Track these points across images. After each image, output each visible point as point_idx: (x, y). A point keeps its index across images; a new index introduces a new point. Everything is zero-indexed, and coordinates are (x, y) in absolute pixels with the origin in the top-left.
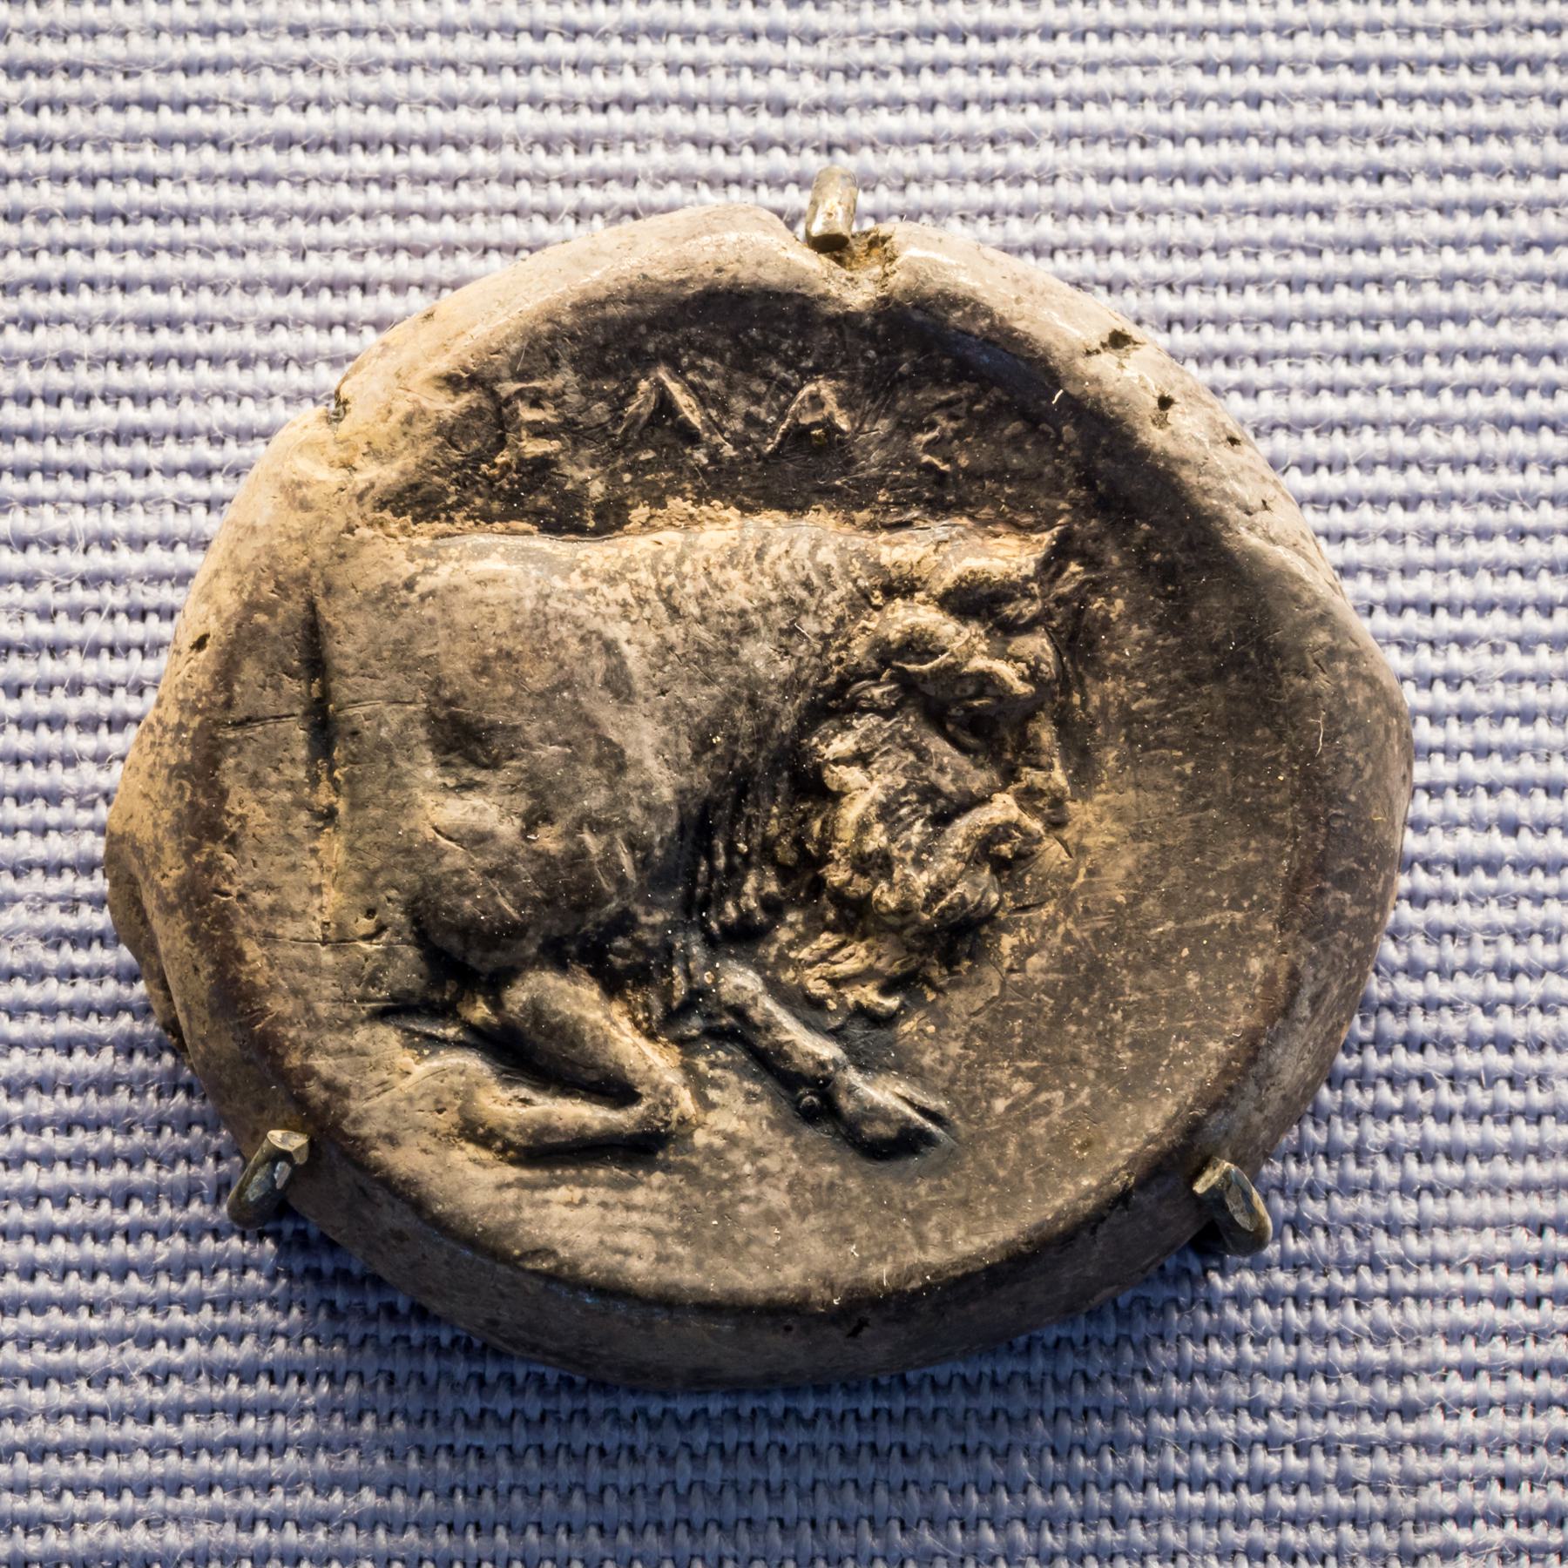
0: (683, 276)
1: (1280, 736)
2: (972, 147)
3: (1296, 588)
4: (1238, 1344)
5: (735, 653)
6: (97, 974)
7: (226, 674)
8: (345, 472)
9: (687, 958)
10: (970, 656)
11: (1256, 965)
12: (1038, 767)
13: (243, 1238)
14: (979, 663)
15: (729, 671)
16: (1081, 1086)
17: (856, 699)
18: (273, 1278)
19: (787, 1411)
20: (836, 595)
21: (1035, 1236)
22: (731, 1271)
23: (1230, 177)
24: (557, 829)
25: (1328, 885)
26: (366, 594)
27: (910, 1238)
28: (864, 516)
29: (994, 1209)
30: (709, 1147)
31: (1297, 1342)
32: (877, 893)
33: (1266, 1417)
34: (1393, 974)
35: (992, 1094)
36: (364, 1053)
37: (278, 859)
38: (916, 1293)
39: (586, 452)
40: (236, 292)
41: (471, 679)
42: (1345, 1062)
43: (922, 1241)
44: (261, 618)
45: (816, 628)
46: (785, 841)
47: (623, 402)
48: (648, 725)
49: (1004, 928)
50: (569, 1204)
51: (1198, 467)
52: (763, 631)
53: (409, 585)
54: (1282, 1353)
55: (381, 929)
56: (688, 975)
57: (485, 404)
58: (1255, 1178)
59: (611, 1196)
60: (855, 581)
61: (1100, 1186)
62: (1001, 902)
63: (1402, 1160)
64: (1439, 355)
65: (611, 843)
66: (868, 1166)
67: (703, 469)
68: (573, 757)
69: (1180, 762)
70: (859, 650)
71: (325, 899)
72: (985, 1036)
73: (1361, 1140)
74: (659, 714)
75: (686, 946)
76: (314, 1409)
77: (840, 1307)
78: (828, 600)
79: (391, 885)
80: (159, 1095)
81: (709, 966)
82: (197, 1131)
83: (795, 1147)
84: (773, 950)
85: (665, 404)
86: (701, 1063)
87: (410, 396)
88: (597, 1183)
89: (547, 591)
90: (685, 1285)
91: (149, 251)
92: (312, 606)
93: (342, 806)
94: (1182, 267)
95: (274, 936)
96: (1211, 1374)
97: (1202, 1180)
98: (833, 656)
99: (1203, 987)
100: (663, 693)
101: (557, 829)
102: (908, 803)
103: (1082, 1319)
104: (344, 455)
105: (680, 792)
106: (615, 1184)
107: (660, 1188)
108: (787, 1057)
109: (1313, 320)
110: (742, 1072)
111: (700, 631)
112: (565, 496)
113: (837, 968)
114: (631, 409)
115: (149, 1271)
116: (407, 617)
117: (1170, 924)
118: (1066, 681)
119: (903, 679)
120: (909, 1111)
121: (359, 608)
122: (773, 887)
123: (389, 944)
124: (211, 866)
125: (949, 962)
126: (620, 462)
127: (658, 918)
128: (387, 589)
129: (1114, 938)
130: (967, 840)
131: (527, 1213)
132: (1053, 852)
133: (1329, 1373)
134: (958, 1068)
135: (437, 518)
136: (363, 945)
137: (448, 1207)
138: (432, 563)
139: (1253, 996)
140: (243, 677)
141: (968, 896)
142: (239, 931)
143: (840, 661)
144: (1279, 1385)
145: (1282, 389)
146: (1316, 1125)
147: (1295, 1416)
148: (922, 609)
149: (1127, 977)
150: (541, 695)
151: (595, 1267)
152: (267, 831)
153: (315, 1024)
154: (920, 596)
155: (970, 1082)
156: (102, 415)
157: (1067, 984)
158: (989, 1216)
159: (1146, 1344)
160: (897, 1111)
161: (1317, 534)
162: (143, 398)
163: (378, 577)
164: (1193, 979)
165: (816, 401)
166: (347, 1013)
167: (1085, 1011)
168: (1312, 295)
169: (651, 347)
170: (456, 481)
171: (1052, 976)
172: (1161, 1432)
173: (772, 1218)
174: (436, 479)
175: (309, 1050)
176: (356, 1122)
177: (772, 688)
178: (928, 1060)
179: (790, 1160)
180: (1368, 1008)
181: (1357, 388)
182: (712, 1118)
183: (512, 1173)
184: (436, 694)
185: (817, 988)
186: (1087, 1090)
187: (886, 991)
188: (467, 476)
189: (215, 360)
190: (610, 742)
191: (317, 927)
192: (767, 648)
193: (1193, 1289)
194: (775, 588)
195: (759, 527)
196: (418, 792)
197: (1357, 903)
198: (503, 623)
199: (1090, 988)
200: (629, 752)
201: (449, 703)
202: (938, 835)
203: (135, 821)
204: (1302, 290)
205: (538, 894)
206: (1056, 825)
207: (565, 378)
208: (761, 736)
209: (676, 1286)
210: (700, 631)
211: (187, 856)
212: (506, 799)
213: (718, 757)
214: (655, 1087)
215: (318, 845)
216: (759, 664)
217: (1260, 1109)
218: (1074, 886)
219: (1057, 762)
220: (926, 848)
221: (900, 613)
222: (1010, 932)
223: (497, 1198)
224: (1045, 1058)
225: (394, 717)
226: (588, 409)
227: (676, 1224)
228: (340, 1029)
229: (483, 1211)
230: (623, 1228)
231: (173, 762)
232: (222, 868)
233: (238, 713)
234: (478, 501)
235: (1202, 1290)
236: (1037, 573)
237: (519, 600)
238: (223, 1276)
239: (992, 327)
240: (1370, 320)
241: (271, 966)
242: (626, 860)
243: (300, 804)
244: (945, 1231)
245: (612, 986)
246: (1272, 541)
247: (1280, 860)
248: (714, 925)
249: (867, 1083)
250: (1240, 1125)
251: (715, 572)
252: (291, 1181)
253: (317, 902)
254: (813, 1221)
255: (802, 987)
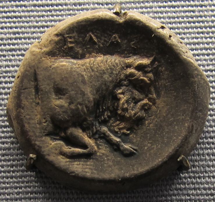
0: (93, 18)
1: (190, 88)
2: (139, 3)
3: (192, 65)
4: (185, 185)
5: (102, 77)
6: (7, 132)
7: (22, 81)
8: (40, 50)
9: (96, 125)
10: (140, 77)
11: (186, 125)
12: (151, 94)
13: (31, 172)
14: (142, 78)
15: (102, 79)
16: (159, 145)
17: (122, 84)
18: (35, 178)
19: (115, 197)
20: (119, 67)
21: (152, 168)
22: (103, 175)
23: (179, 7)
24: (74, 105)
25: (198, 112)
26: (43, 68)
27: (132, 169)
28: (123, 55)
29: (145, 164)
30: (99, 155)
31: (194, 184)
32: (126, 115)
33: (190, 196)
34: (208, 127)
35: (144, 146)
36: (44, 141)
37: (30, 111)
38: (133, 178)
39: (79, 46)
41: (60, 81)
42: (201, 141)
43: (134, 170)
44: (27, 73)
45: (115, 73)
46: (111, 107)
47: (85, 38)
48: (89, 88)
49: (146, 120)
50: (77, 165)
51: (176, 46)
52: (107, 73)
53: (50, 67)
54: (192, 186)
55: (46, 121)
56: (96, 128)
57: (62, 38)
58: (187, 158)
59: (84, 163)
60: (122, 66)
61: (162, 160)
62: (146, 116)
63: (210, 156)
64: (212, 33)
65: (83, 107)
66: (125, 158)
67: (97, 49)
68: (77, 93)
69: (174, 93)
70: (122, 76)
71: (38, 117)
72: (143, 137)
73: (203, 152)
74: (90, 86)
75: (96, 124)
76: (42, 198)
77: (120, 180)
78: (117, 68)
79: (48, 114)
80: (17, 150)
81: (99, 127)
82: (23, 156)
83: (113, 155)
84: (110, 124)
85: (91, 38)
86: (98, 142)
87: (51, 37)
88: (82, 161)
89: (72, 67)
90: (95, 177)
91: (14, 22)
92: (35, 70)
93: (40, 102)
94: (172, 20)
95: (30, 123)
96: (181, 189)
97: (179, 159)
98: (118, 77)
99: (178, 128)
100: (91, 83)
101: (74, 105)
102: (130, 100)
103: (161, 182)
104: (40, 47)
105: (94, 99)
106: (84, 161)
107: (92, 162)
108: (112, 141)
109: (192, 28)
110: (105, 143)
111: (97, 73)
112: (76, 53)
113: (120, 127)
114: (86, 39)
115: (16, 177)
116: (50, 72)
117: (173, 119)
118: (155, 81)
119: (129, 80)
120: (131, 149)
121: (42, 70)
122: (109, 114)
123: (48, 124)
124: (19, 112)
125: (138, 125)
126: (84, 47)
127: (91, 119)
128: (47, 67)
129: (164, 121)
130: (140, 106)
131: (70, 166)
132: (154, 108)
133: (199, 189)
134: (139, 142)
135: (55, 57)
136: (44, 124)
137: (58, 165)
138: (54, 63)
139: (186, 130)
140: (24, 82)
141: (140, 115)
142: (24, 122)
143: (119, 78)
144: (192, 191)
145: (188, 38)
146: (196, 151)
147: (194, 196)
148: (132, 70)
149: (166, 127)
150: (71, 84)
151: (81, 175)
152: (28, 106)
153: (36, 137)
154: (132, 67)
155: (141, 144)
156: (8, 47)
157: (156, 129)
158: (144, 165)
159: (171, 185)
160: (129, 149)
162: (14, 44)
163: (46, 65)
164: (176, 127)
165: (115, 37)
166: (41, 135)
167: (159, 133)
168: (192, 24)
169: (89, 29)
170: (58, 51)
171: (154, 127)
172: (174, 199)
173: (110, 166)
174: (55, 50)
175: (35, 141)
176: (43, 152)
177: (109, 82)
178: (134, 141)
179: (113, 157)
180: (204, 132)
181: (199, 38)
182: (100, 151)
183: (68, 160)
184: (55, 84)
185: (116, 130)
186: (160, 145)
187: (127, 130)
188: (60, 49)
189: (25, 38)
190: (82, 91)
191: (36, 121)
192: (107, 76)
193: (178, 176)
194: (109, 66)
195: (106, 57)
196: (52, 99)
197: (202, 115)
198: (65, 72)
199: (160, 129)
200: (86, 92)
201: (57, 85)
202: (135, 105)
203: (10, 106)
204: (191, 24)
205: (71, 115)
206: (154, 104)
207: (75, 34)
208: (107, 90)
209: (95, 178)
210: (97, 73)
211: (16, 111)
212: (66, 100)
213: (100, 93)
214: (91, 146)
215: (37, 108)
216: (106, 78)
217: (187, 148)
218: (157, 113)
219: (154, 94)
220: (133, 107)
221: (129, 70)
222: (147, 120)
223: (65, 164)
224: (153, 140)
225: (48, 87)
226: (79, 39)
227: (94, 168)
228: (40, 137)
229: (63, 166)
230: (86, 168)
231: (14, 96)
232: (21, 112)
233: (24, 88)
234: (62, 54)
235: (179, 176)
236: (150, 63)
237: (68, 69)
238: (28, 178)
239: (142, 24)
240: (201, 28)
241: (29, 127)
242: (85, 110)
243: (33, 102)
244: (137, 168)
245: (84, 130)
246: (188, 57)
247: (190, 108)
248: (100, 120)
249: (125, 145)
250: (184, 150)
251: (99, 64)
252: (33, 162)
253: (36, 117)
254: (116, 167)
255: (114, 130)
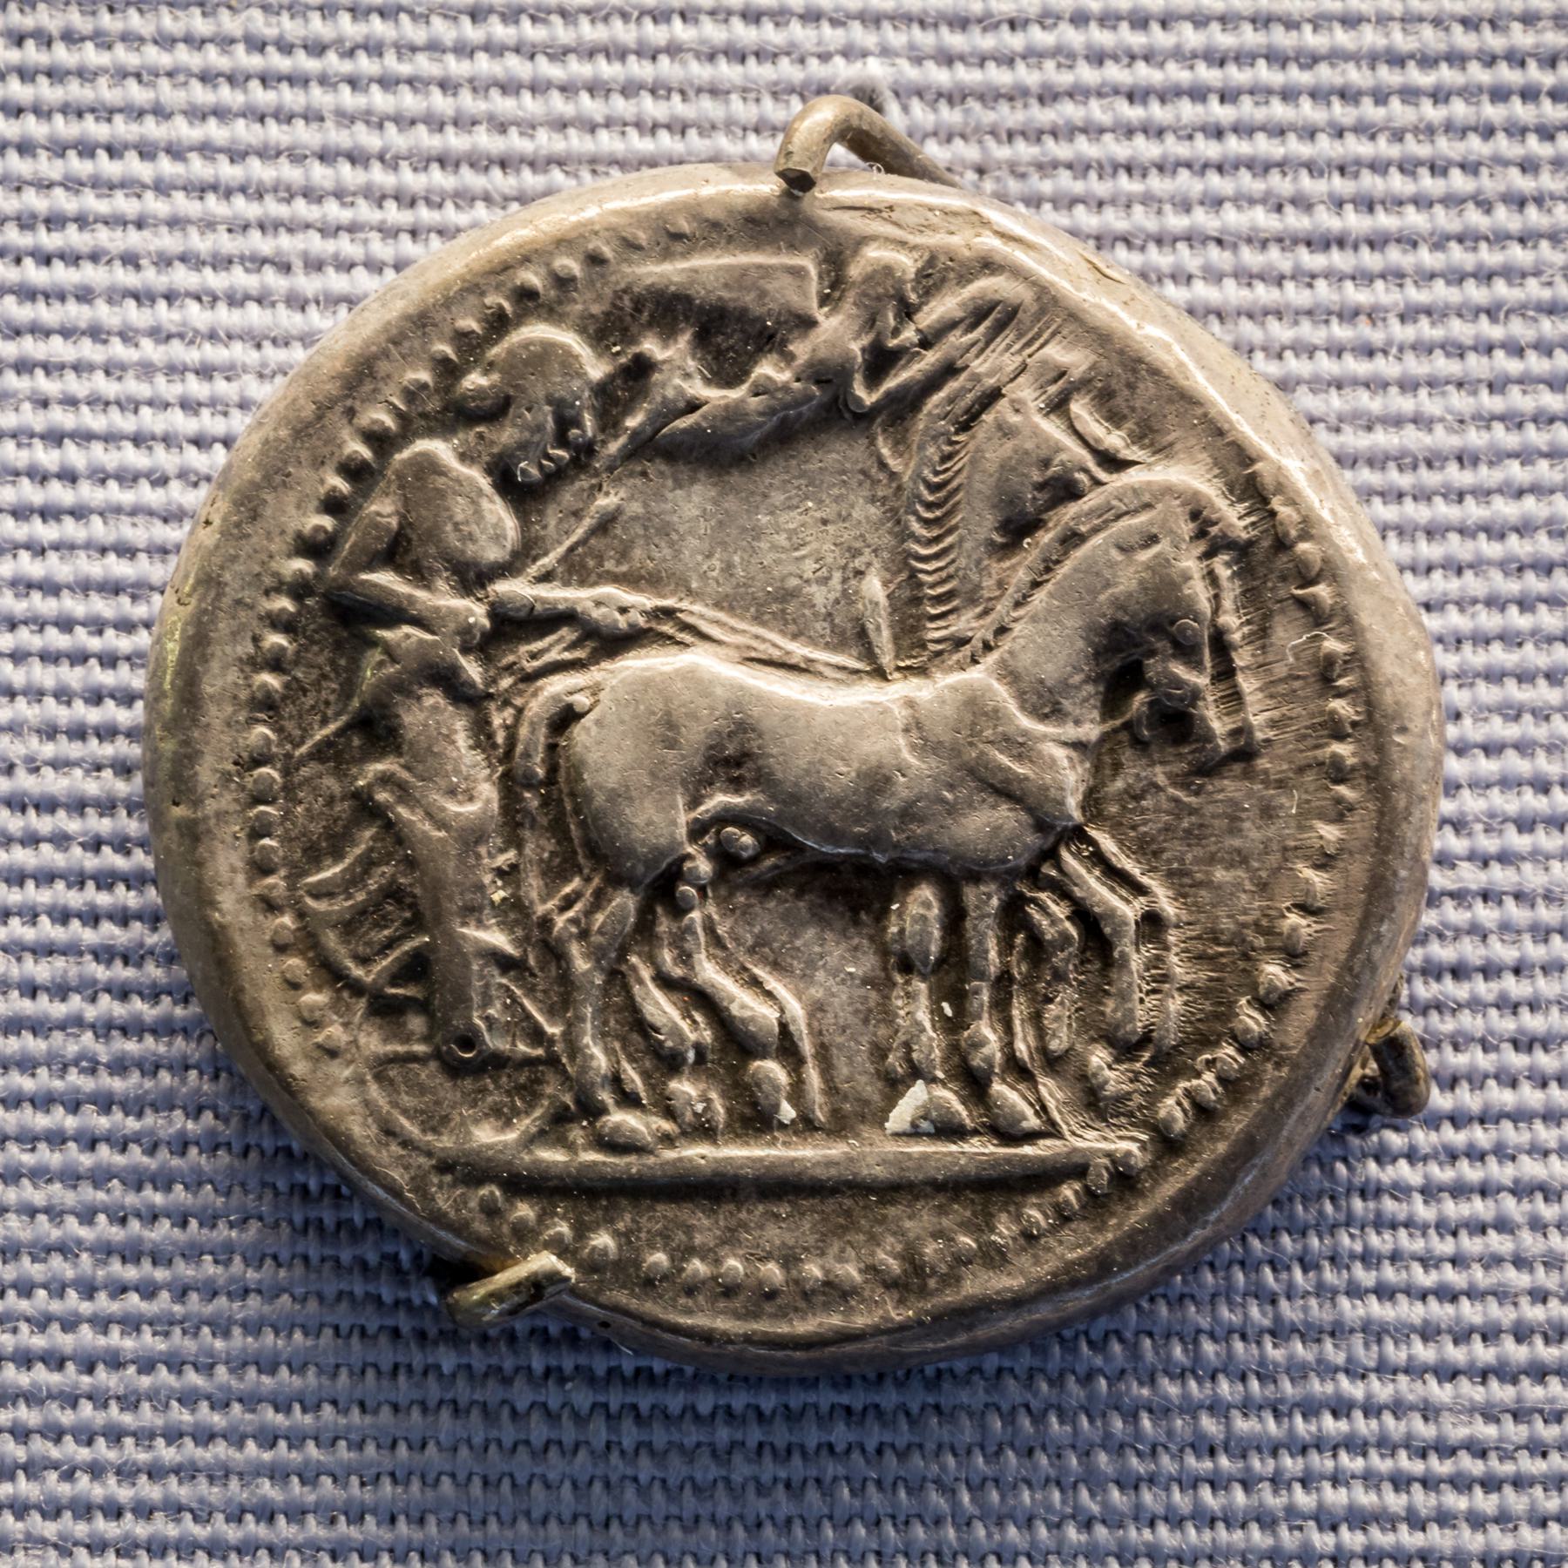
40: (1394, 390)
161: (1402, 570)
